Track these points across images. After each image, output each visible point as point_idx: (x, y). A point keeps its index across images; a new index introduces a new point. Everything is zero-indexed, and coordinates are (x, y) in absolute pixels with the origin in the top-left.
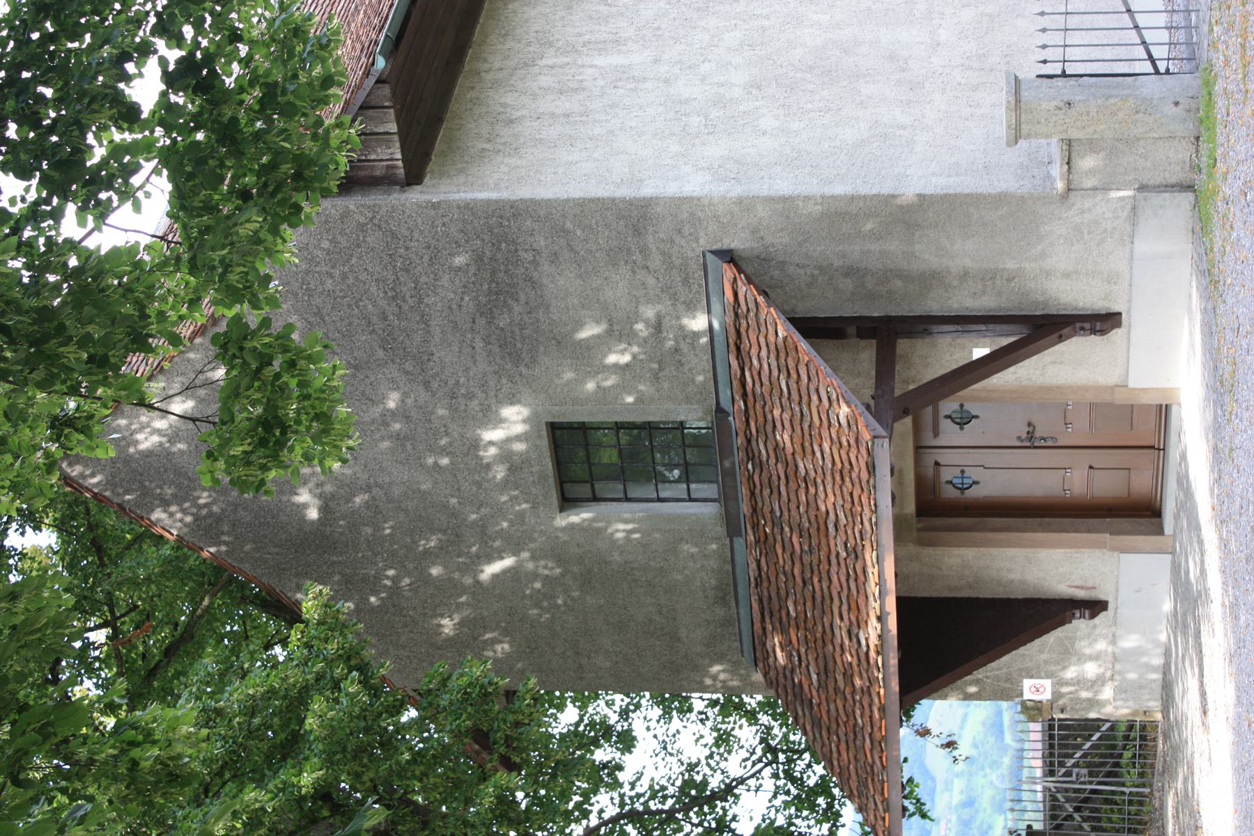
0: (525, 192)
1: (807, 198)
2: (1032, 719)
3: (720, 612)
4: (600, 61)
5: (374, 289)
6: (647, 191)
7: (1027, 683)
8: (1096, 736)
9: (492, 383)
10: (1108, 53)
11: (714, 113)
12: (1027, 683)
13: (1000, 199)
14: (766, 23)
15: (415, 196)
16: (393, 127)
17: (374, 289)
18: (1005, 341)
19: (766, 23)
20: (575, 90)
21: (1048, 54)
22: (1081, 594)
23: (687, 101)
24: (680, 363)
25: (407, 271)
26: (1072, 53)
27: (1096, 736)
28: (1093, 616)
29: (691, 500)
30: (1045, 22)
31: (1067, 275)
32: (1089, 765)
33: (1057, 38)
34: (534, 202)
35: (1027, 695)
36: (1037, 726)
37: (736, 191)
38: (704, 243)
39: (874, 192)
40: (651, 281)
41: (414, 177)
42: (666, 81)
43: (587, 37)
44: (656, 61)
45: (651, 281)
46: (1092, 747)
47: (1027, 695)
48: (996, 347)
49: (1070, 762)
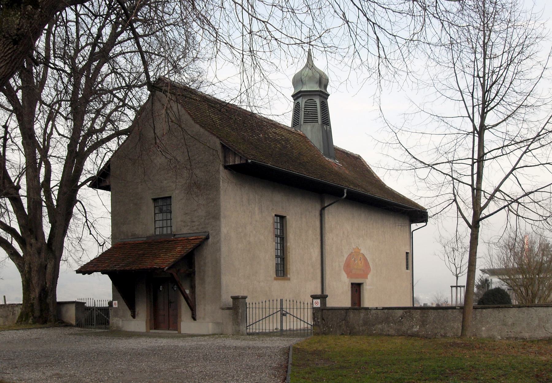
0: (222, 192)
1: (220, 254)
2: (109, 303)
3: (130, 234)
4: (256, 209)
5: (201, 157)
6: (222, 220)
7: (117, 302)
8: (106, 317)
9: (180, 184)
10: (251, 316)
11: (242, 234)
12: (117, 302)
13: (220, 296)
14: (266, 245)
15: (221, 168)
16: (236, 163)
17: (201, 157)
18: (180, 293)
19: (266, 245)
20: (249, 203)
21: (254, 305)
22: (136, 313)
23: (246, 228)
24: (185, 226)
25: (205, 165)
26: (251, 309)
27: (106, 317)
28: (132, 316)
29: (155, 228)
30: (257, 303)
31: (204, 309)
32: (98, 315)
33: (257, 306)
34: (220, 194)
35: (114, 302)
36: (107, 306)
37: (222, 239)
38: (211, 232)
39: (222, 269)
40: (202, 220)
41: (226, 167)
42: (251, 223)
43: (263, 205)
44: (256, 221)
45: (202, 220)
46: (105, 318)
47: (114, 302)
48: (188, 295)
49: (99, 311)
